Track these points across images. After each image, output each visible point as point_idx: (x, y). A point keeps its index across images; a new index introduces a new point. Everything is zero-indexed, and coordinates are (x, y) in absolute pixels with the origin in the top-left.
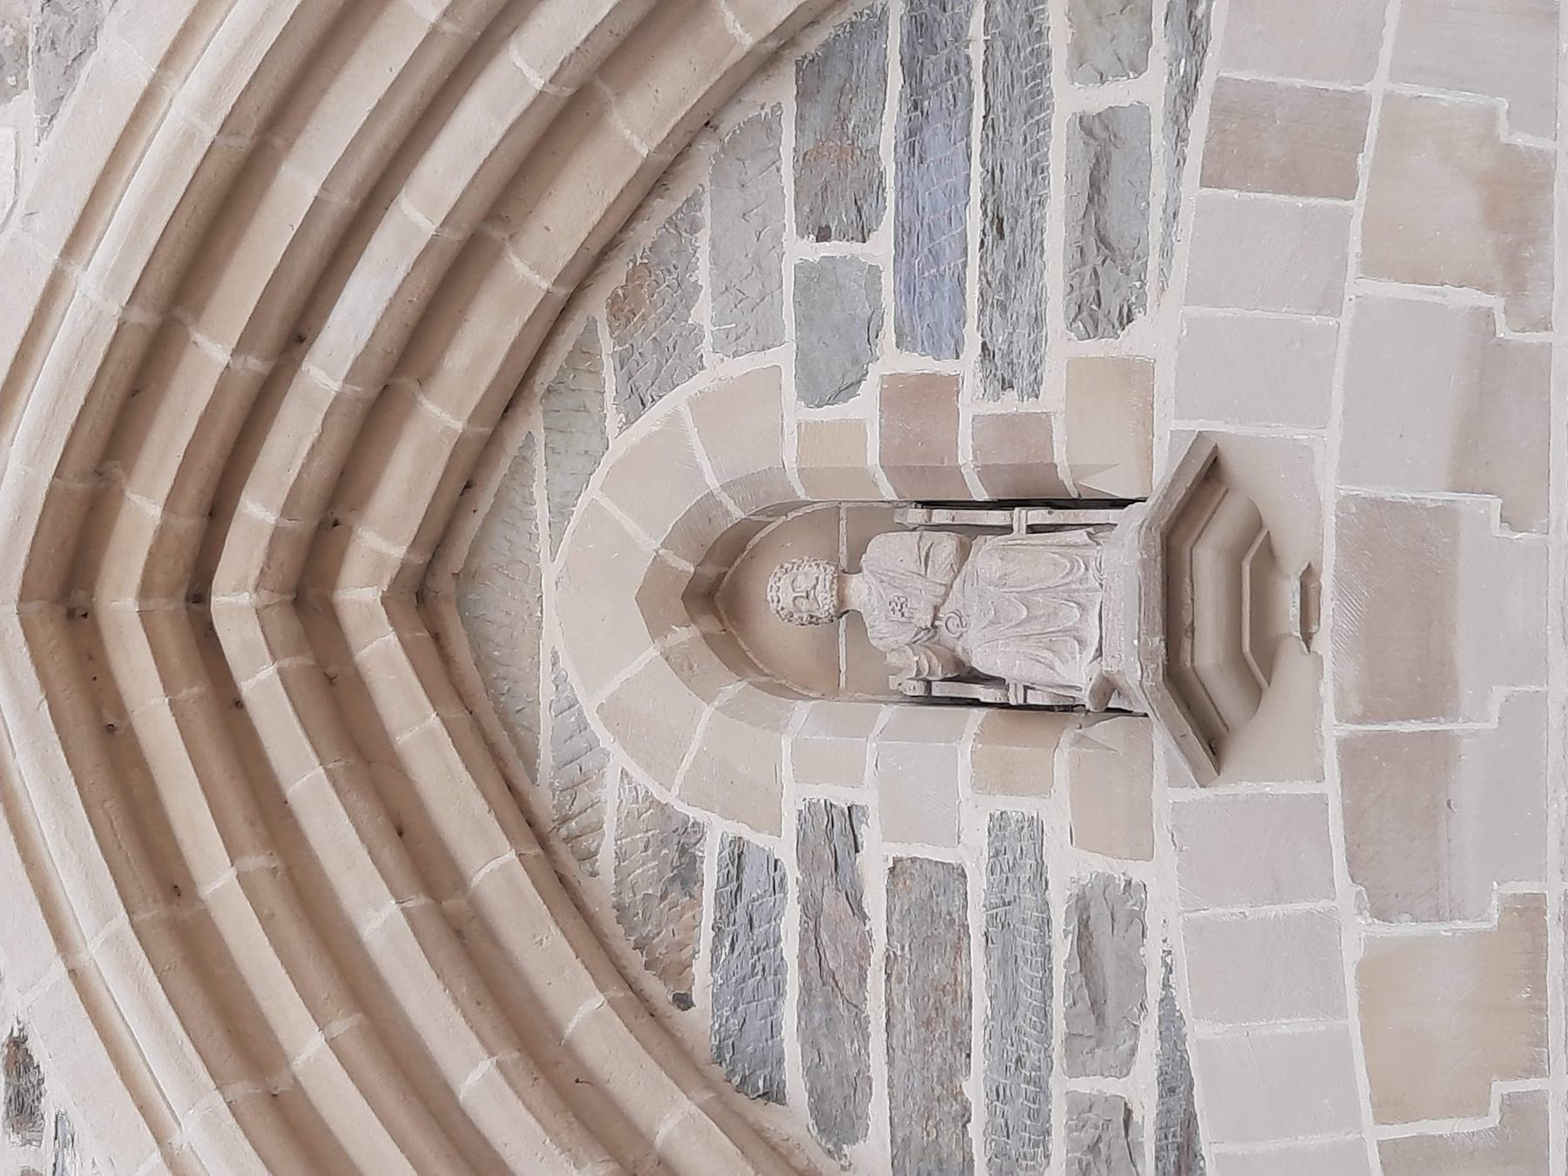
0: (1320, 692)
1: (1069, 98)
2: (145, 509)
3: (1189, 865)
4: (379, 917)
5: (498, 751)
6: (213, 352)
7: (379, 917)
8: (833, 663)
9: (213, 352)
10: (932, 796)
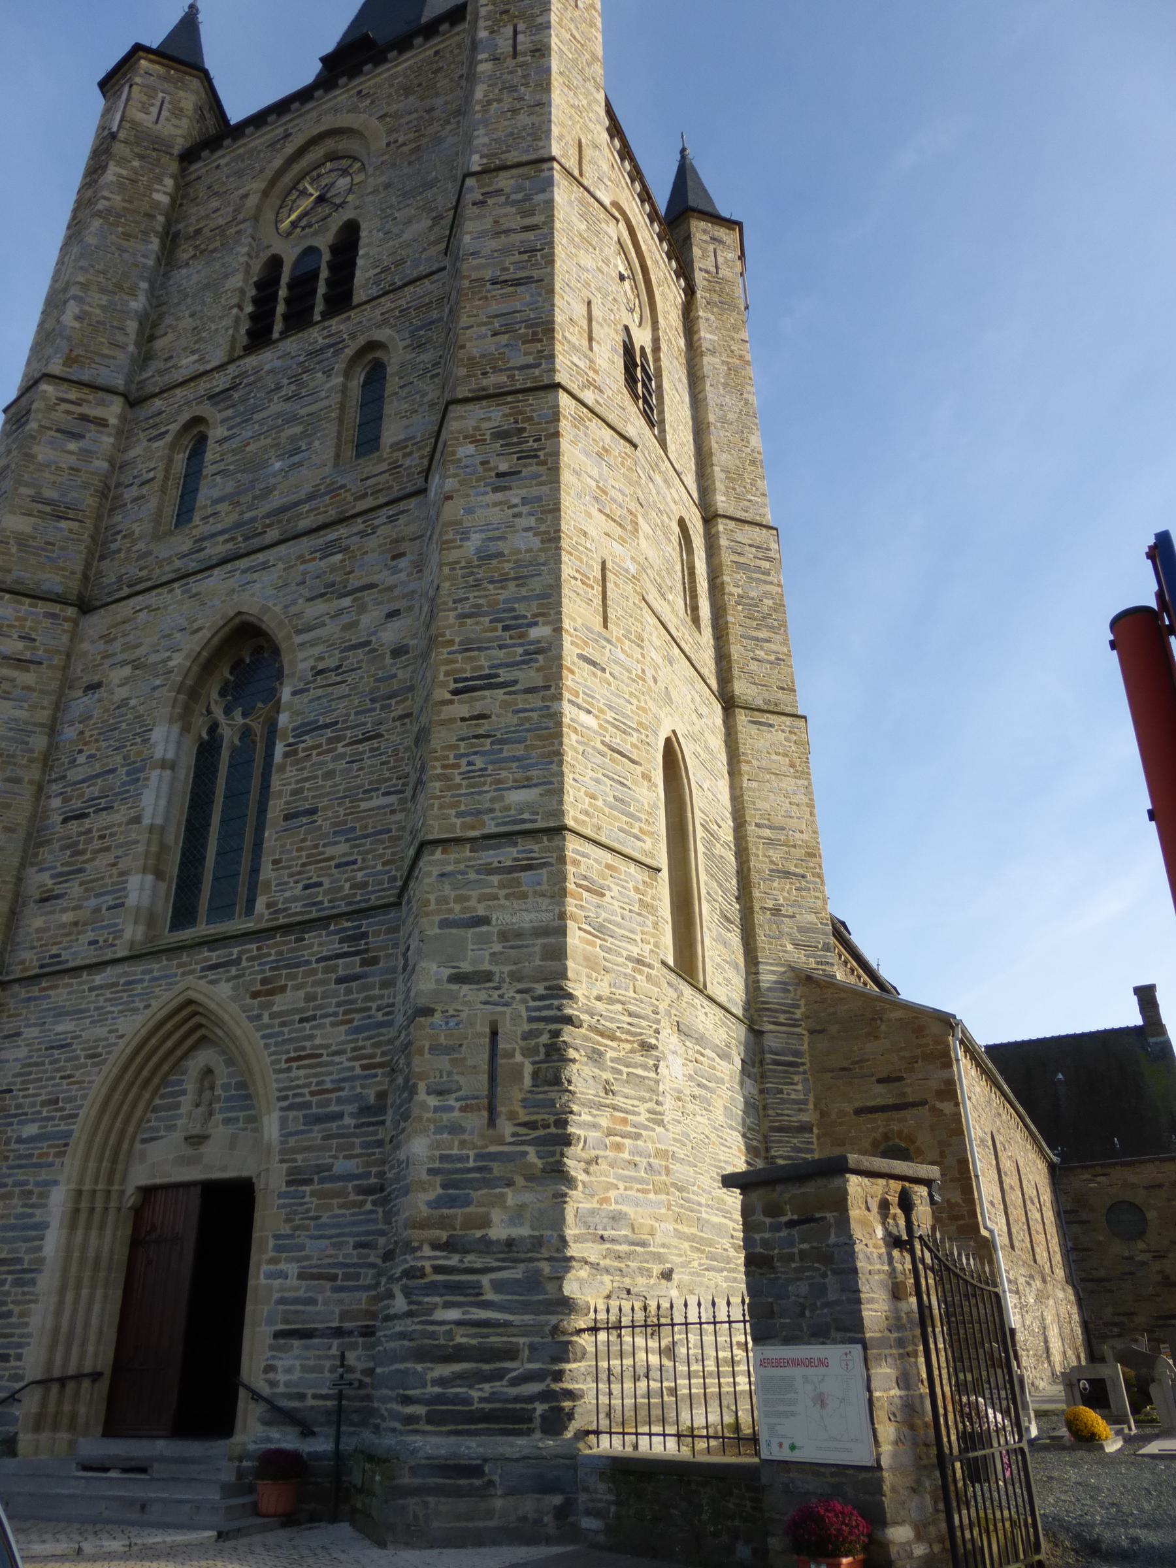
0: (188, 1151)
1: (241, 1114)
4: (169, 1044)
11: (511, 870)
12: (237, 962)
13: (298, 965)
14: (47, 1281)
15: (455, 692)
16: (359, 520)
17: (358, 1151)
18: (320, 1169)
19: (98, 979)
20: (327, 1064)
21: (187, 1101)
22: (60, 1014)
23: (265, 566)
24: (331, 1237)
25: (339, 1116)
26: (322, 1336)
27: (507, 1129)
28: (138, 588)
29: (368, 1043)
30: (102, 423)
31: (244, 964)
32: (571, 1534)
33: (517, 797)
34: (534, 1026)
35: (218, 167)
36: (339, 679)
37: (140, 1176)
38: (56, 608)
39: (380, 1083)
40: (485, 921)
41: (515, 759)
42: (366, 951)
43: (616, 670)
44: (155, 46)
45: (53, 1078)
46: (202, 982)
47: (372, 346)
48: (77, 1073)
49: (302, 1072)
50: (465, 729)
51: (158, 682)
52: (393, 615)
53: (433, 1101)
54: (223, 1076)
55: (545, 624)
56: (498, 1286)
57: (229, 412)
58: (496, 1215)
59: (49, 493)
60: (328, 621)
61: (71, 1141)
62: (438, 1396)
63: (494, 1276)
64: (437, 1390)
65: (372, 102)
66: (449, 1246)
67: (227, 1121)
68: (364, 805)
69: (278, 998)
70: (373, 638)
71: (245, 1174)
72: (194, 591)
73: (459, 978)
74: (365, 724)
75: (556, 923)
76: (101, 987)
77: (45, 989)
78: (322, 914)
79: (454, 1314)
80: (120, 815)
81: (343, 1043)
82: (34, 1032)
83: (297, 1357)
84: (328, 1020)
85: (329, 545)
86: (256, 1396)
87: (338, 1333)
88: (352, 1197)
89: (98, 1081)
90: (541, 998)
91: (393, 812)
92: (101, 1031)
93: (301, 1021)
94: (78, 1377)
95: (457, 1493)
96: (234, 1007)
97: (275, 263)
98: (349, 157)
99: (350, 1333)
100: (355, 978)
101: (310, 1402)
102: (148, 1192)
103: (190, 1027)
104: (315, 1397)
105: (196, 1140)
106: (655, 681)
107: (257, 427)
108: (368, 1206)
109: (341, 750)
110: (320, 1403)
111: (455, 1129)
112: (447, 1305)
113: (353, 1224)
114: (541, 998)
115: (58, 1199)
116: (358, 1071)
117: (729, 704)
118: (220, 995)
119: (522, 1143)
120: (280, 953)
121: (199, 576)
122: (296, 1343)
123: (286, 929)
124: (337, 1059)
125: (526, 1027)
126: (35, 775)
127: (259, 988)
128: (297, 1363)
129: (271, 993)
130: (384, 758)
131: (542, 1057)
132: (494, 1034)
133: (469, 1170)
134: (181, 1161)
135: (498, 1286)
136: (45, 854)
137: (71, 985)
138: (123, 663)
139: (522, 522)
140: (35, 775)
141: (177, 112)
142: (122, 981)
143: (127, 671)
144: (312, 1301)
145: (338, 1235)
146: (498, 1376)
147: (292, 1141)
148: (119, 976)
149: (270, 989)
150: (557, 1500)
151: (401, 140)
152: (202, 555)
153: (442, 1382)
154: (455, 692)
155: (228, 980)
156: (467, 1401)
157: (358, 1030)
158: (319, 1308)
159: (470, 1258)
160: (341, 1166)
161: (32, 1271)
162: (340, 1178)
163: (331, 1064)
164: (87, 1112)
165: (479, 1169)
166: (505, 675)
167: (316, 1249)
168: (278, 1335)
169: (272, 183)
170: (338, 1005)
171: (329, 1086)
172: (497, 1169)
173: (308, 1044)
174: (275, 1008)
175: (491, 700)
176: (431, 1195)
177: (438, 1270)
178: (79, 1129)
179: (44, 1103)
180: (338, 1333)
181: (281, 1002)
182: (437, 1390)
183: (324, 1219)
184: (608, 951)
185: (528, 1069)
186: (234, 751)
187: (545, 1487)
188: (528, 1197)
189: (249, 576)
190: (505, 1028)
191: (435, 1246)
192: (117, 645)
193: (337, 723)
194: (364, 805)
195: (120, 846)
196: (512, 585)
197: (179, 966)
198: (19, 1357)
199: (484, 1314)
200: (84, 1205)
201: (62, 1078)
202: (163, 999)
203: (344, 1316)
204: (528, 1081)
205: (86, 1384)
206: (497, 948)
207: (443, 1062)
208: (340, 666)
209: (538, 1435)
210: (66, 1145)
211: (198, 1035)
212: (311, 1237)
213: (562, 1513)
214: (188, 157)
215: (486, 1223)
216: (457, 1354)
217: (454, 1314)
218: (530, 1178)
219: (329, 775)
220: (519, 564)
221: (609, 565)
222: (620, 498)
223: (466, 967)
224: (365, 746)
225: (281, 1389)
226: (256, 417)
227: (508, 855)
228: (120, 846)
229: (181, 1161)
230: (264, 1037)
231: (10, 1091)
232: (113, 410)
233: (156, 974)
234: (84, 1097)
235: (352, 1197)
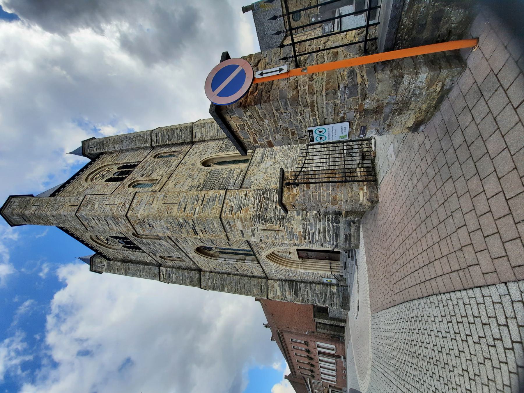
11: (230, 226)
14: (315, 272)
21: (283, 254)
27: (281, 228)
30: (166, 270)
32: (359, 222)
33: (216, 225)
37: (297, 259)
38: (202, 275)
40: (241, 231)
41: (208, 225)
43: (186, 200)
44: (89, 266)
50: (204, 233)
53: (278, 240)
56: (312, 230)
58: (298, 230)
59: (181, 278)
66: (305, 238)
73: (254, 235)
86: (334, 249)
89: (281, 267)
94: (330, 266)
95: (350, 239)
96: (266, 252)
97: (123, 246)
102: (299, 257)
106: (190, 169)
112: (316, 238)
117: (192, 143)
126: (231, 276)
132: (264, 230)
134: (294, 254)
139: (159, 223)
140: (231, 276)
141: (101, 262)
153: (330, 239)
166: (192, 226)
169: (108, 247)
172: (289, 230)
175: (198, 229)
176: (295, 240)
177: (309, 239)
178: (290, 269)
184: (244, 205)
185: (269, 224)
187: (349, 225)
188: (294, 225)
196: (173, 225)
199: (317, 232)
204: (272, 225)
207: (270, 238)
213: (354, 223)
214: (109, 259)
215: (300, 232)
217: (317, 237)
218: (291, 225)
220: (168, 223)
221: (163, 202)
222: (148, 198)
223: (251, 234)
227: (227, 227)
232: (163, 269)
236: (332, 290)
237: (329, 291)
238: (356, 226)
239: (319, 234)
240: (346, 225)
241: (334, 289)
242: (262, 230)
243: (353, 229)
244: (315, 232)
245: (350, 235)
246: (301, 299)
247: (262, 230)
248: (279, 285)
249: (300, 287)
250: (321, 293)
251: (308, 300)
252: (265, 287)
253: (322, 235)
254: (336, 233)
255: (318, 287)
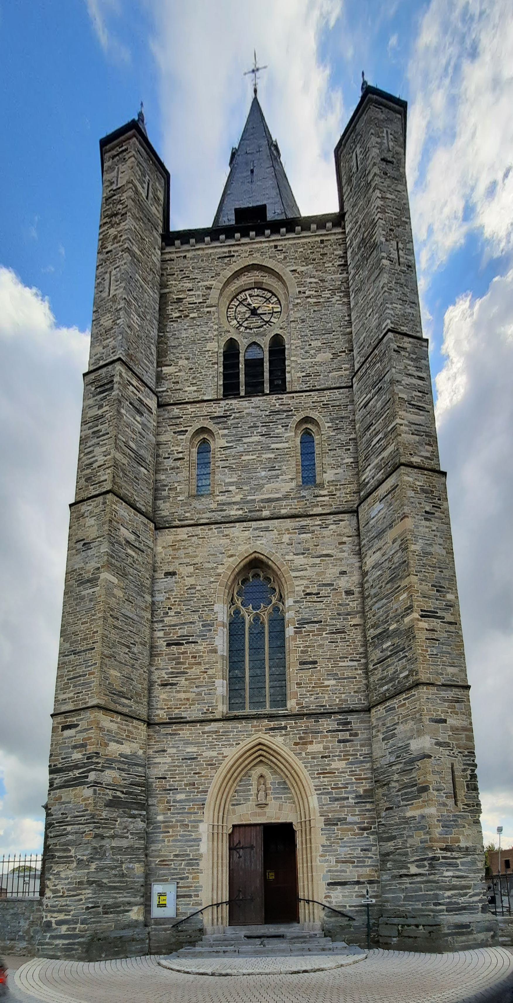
0: (259, 810)
1: (283, 796)
2: (265, 748)
3: (252, 803)
4: (246, 762)
5: (254, 766)
6: (272, 752)
7: (246, 762)
8: (259, 784)
9: (272, 752)
10: (253, 791)
12: (285, 728)
13: (318, 733)
15: (422, 616)
16: (318, 518)
17: (357, 813)
18: (339, 820)
19: (207, 728)
20: (337, 777)
22: (187, 743)
23: (267, 529)
24: (350, 846)
25: (347, 798)
26: (351, 884)
27: (461, 806)
28: (186, 522)
29: (357, 769)
31: (289, 729)
34: (465, 767)
35: (185, 257)
36: (319, 600)
39: (364, 786)
40: (445, 721)
42: (352, 730)
45: (190, 773)
46: (267, 735)
47: (307, 420)
48: (203, 772)
49: (326, 779)
51: (212, 580)
52: (343, 573)
53: (436, 793)
54: (270, 778)
55: (452, 593)
57: (226, 431)
60: (308, 568)
61: (206, 803)
62: (449, 902)
63: (461, 860)
64: (448, 900)
65: (285, 258)
66: (446, 849)
67: (276, 798)
68: (341, 664)
69: (309, 746)
70: (335, 583)
71: (289, 821)
72: (225, 533)
74: (336, 625)
75: (469, 726)
76: (210, 732)
77: (175, 730)
78: (325, 711)
79: (450, 874)
80: (202, 647)
81: (345, 768)
82: (174, 750)
83: (341, 892)
84: (336, 758)
85: (303, 527)
87: (358, 883)
88: (357, 831)
90: (466, 756)
91: (356, 669)
92: (214, 754)
93: (322, 757)
94: (222, 903)
95: (462, 934)
98: (270, 291)
99: (363, 883)
100: (348, 741)
101: (348, 908)
103: (261, 754)
104: (350, 906)
105: (262, 806)
107: (246, 447)
108: (365, 835)
109: (324, 635)
110: (353, 908)
111: (445, 805)
112: (447, 870)
113: (358, 842)
114: (466, 756)
115: (204, 829)
116: (354, 781)
118: (278, 741)
119: (466, 812)
120: (308, 726)
121: (227, 525)
122: (339, 887)
123: (309, 715)
124: (343, 775)
125: (463, 767)
127: (298, 741)
128: (341, 894)
129: (305, 744)
130: (348, 643)
131: (469, 779)
133: (451, 821)
134: (254, 814)
135: (463, 864)
136: (159, 661)
137: (191, 730)
138: (188, 565)
142: (221, 730)
143: (191, 569)
144: (345, 871)
145: (353, 846)
146: (465, 894)
147: (325, 808)
148: (221, 728)
149: (303, 742)
150: (492, 933)
151: (308, 293)
152: (224, 513)
153: (449, 897)
154: (422, 616)
155: (281, 736)
156: (458, 904)
157: (351, 763)
158: (348, 874)
159: (454, 853)
160: (350, 819)
161: (196, 860)
162: (350, 823)
163: (341, 777)
164: (213, 790)
165: (453, 821)
167: (343, 852)
168: (329, 884)
170: (341, 752)
171: (340, 786)
173: (328, 768)
174: (308, 751)
177: (444, 858)
179: (186, 785)
180: (358, 883)
181: (311, 748)
182: (448, 900)
183: (345, 839)
186: (251, 624)
187: (488, 930)
188: (470, 832)
189: (257, 533)
190: (456, 766)
191: (441, 849)
192: (181, 553)
193: (321, 622)
194: (341, 664)
195: (208, 663)
197: (252, 727)
198: (197, 896)
200: (216, 831)
201: (194, 773)
202: (247, 743)
203: (359, 876)
205: (224, 905)
206: (450, 733)
208: (319, 593)
209: (480, 914)
210: (203, 804)
211: (258, 759)
212: (341, 847)
215: (458, 841)
216: (454, 888)
217: (450, 874)
219: (321, 646)
224: (338, 636)
225: (334, 904)
226: (245, 440)
228: (208, 663)
229: (254, 814)
230: (303, 763)
231: (166, 778)
233: (240, 729)
234: (210, 783)
235: (357, 831)
236: (135, 909)
237: (132, 900)
238: (487, 940)
239: (457, 877)
240: (487, 924)
241: (135, 914)
242: (452, 765)
243: (481, 936)
244: (459, 870)
245: (470, 933)
246: (104, 814)
247: (452, 765)
248: (134, 754)
249: (134, 817)
250: (123, 875)
251: (103, 838)
252: (126, 710)
253: (455, 882)
254: (464, 908)
255: (138, 869)
